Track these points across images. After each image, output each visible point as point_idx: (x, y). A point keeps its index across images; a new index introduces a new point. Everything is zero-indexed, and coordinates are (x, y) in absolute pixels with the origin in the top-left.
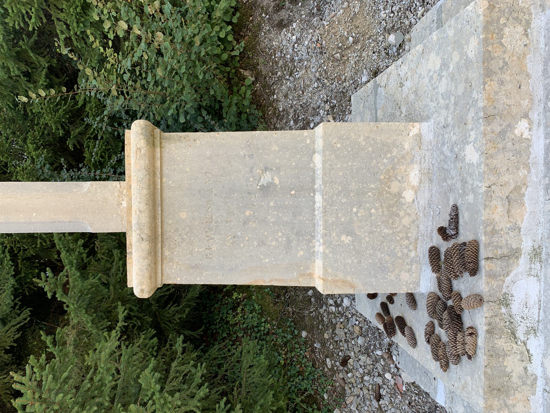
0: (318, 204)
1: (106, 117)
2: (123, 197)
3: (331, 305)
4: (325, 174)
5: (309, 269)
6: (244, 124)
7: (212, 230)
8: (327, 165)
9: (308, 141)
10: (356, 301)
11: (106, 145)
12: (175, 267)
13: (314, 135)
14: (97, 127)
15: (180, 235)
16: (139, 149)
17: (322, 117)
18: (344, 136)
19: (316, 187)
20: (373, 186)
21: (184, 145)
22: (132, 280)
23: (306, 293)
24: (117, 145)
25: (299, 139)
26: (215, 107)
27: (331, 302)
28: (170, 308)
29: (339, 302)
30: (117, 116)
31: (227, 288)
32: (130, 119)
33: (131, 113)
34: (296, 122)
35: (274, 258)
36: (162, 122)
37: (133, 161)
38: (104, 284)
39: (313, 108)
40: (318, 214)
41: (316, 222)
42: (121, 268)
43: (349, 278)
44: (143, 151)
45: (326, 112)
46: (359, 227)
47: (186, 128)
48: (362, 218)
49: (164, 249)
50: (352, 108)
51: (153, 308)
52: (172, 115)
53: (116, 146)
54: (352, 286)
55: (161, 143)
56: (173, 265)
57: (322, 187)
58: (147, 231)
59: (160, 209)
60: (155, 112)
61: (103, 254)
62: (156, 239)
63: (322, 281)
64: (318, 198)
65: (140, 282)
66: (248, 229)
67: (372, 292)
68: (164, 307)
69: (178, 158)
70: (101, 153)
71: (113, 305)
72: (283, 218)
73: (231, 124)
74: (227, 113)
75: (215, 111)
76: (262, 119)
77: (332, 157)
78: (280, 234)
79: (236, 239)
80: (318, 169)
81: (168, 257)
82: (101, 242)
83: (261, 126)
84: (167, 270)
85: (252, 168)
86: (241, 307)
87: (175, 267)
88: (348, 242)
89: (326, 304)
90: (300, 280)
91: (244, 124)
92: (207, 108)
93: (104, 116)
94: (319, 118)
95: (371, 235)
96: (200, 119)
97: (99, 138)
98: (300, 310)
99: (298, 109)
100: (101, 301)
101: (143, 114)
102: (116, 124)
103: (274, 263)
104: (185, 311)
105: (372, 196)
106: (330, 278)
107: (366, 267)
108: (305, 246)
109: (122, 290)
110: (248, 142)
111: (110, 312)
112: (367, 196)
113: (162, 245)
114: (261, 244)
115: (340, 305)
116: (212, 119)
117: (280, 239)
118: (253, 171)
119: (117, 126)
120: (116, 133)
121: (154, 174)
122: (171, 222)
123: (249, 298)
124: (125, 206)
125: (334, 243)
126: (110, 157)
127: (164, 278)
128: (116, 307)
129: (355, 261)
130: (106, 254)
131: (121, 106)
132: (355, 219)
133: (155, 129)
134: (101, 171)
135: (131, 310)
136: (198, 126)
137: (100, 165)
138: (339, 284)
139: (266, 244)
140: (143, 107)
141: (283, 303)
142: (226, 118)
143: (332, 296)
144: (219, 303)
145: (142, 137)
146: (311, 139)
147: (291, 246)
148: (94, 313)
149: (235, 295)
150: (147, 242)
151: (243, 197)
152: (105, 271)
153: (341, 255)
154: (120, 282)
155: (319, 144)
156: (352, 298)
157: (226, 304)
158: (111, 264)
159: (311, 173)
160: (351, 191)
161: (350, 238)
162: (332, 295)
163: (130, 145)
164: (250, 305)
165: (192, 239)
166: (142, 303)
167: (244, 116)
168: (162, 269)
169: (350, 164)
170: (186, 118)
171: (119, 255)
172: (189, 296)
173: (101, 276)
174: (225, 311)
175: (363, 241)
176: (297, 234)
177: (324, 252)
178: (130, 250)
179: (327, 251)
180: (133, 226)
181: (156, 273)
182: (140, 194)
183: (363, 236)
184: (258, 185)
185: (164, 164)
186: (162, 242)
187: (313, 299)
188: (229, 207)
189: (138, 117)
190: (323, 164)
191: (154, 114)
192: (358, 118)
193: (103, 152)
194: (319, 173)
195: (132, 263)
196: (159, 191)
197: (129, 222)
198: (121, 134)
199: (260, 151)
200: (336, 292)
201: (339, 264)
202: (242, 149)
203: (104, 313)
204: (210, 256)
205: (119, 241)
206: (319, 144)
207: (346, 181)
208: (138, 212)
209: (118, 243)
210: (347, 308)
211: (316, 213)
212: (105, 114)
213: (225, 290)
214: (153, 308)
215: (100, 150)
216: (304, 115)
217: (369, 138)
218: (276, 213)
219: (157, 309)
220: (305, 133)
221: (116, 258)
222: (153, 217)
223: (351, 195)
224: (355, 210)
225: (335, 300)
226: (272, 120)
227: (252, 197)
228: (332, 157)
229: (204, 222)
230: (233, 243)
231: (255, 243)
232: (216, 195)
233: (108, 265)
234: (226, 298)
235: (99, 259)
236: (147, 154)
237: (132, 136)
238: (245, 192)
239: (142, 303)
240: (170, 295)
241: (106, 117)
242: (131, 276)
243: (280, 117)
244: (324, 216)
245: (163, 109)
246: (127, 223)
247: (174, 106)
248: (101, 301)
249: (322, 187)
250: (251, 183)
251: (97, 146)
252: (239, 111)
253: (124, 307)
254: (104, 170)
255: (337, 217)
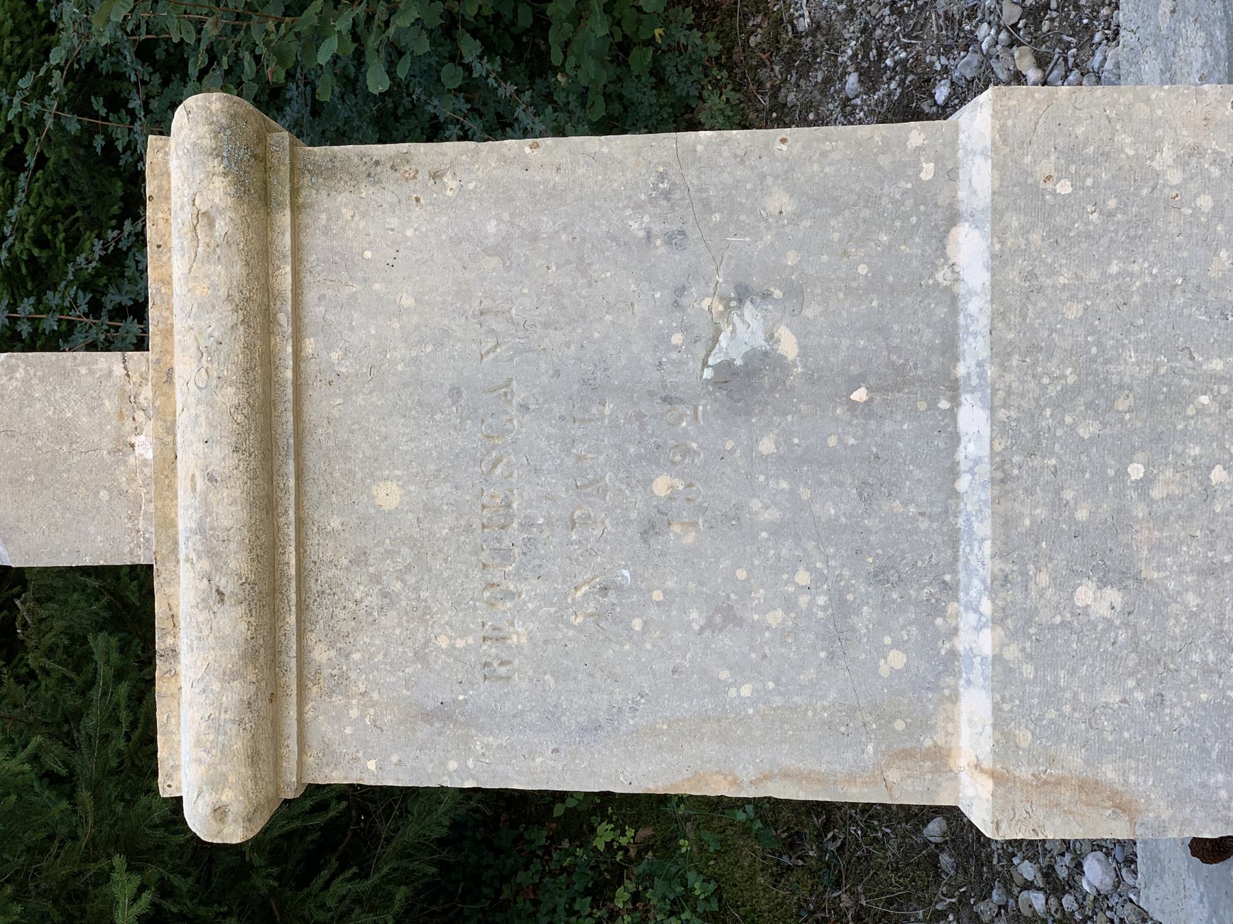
0: (971, 448)
1: (57, 74)
2: (140, 416)
3: (1028, 886)
4: (1003, 315)
5: (932, 729)
6: (642, 95)
7: (506, 556)
8: (1013, 275)
9: (928, 172)
10: (1141, 868)
11: (58, 193)
12: (354, 713)
13: (953, 144)
14: (19, 116)
15: (376, 579)
16: (205, 218)
17: (988, 56)
18: (1085, 146)
19: (961, 370)
20: (1217, 365)
21: (390, 197)
22: (176, 768)
23: (917, 830)
24: (121, 194)
25: (884, 161)
26: (514, 24)
27: (1027, 870)
28: (327, 886)
29: (1063, 873)
30: (105, 67)
31: (571, 803)
32: (156, 79)
33: (160, 54)
34: (870, 79)
35: (777, 681)
36: (293, 91)
37: (178, 265)
38: (51, 778)
39: (948, 18)
40: (972, 488)
41: (961, 522)
42: (124, 715)
43: (1109, 773)
44: (222, 226)
45: (1003, 36)
46: (1157, 547)
47: (399, 120)
48: (1168, 506)
49: (312, 638)
50: (1121, 17)
51: (257, 881)
52: (336, 58)
53: (100, 195)
54: (1123, 806)
55: (295, 192)
56: (347, 706)
57: (990, 371)
58: (238, 561)
59: (291, 467)
60: (261, 50)
61: (50, 652)
62: (277, 593)
63: (989, 784)
64: (973, 419)
65: (206, 775)
66: (662, 554)
67: (1210, 832)
68: (303, 881)
69: (368, 254)
70: (38, 227)
71: (93, 868)
72: (817, 508)
73: (583, 95)
74: (567, 44)
75: (516, 38)
76: (721, 67)
77: (1035, 237)
78: (803, 577)
79: (612, 597)
80: (972, 293)
81: (327, 672)
82: (38, 601)
83: (715, 101)
84: (322, 726)
85: (681, 290)
86: (631, 887)
87: (354, 713)
88: (1107, 613)
89: (1008, 882)
90: (893, 775)
91: (642, 95)
92: (482, 24)
93: (49, 71)
94: (972, 58)
95: (1211, 582)
96: (451, 76)
97: (31, 161)
98: (889, 903)
99: (880, 21)
100: (40, 849)
101: (213, 58)
102: (98, 104)
103: (778, 701)
104: (390, 897)
105: (1215, 408)
106: (1024, 772)
107: (1185, 721)
108: (914, 630)
109: (129, 804)
110: (662, 177)
111: (79, 896)
112: (1190, 411)
113: (299, 621)
114: (718, 619)
115: (1071, 885)
116: (504, 77)
117: (804, 600)
118: (684, 301)
119: (103, 112)
120: (99, 142)
121: (266, 318)
122: (335, 523)
123: (666, 846)
124: (149, 455)
125: (1044, 616)
126: (73, 245)
127: (310, 760)
128: (104, 877)
129: (1139, 696)
130: (59, 653)
131: (122, 26)
132: (1140, 511)
133: (270, 130)
134: (39, 301)
135: (165, 890)
136: (444, 107)
137: (32, 277)
138: (1065, 796)
139: (739, 622)
140: (211, 30)
141: (812, 873)
142: (562, 69)
143: (1032, 849)
144: (537, 865)
145: (216, 165)
146: (938, 160)
147: (853, 629)
148: (14, 899)
149: (604, 834)
150: (241, 610)
151: (640, 416)
152: (59, 725)
153: (1073, 672)
154: (116, 772)
155: (978, 180)
156: (1122, 855)
157: (563, 870)
158: (83, 693)
159: (941, 312)
160: (1121, 387)
161: (1113, 595)
162: (1031, 842)
163: (167, 199)
164: (669, 879)
165: (424, 595)
166: (211, 860)
167: (641, 59)
168: (301, 721)
169: (1114, 269)
170: (391, 73)
171: (115, 656)
172: (410, 833)
173: (40, 745)
174: (562, 902)
175: (1174, 608)
176: (878, 576)
177: (997, 659)
178: (170, 641)
179: (1012, 653)
180: (181, 540)
181: (276, 739)
182: (211, 405)
183: (1171, 585)
184: (705, 364)
185: (308, 278)
186: (302, 607)
187: (945, 860)
188: (580, 458)
189: (193, 71)
190: (993, 272)
191: (257, 59)
192: (1150, 65)
193: (44, 221)
194: (976, 309)
195: (176, 696)
196: (290, 391)
197: (167, 524)
198: (120, 146)
199: (717, 217)
200: (1055, 829)
201: (1067, 709)
202: (639, 207)
203: (55, 902)
204: (503, 670)
205: (121, 602)
206: (978, 180)
207: (1099, 344)
208: (200, 484)
209: (109, 607)
210: (1100, 897)
211: (963, 484)
212: (53, 63)
213: (559, 810)
214: (257, 881)
215: (33, 211)
216: (905, 47)
217: (1202, 155)
218: (784, 485)
219: (271, 889)
220: (915, 133)
221: (104, 672)
222: (265, 504)
223: (1122, 405)
224: (1136, 471)
225: (1044, 862)
226: (763, 73)
227: (681, 418)
228: (1035, 237)
229: (477, 524)
230: (598, 616)
231: (694, 615)
232: (524, 408)
233: (71, 701)
234: (566, 844)
235: (32, 675)
236: (239, 237)
237: (173, 164)
238: (651, 394)
239: (211, 860)
240: (332, 827)
241: (57, 74)
242: (175, 751)
243: (797, 59)
244: (996, 500)
245: (298, 35)
246: (158, 526)
247: (343, 24)
248: (40, 849)
249: (990, 371)
250: (674, 355)
251: (21, 196)
252: (618, 39)
253: (136, 880)
254: (52, 299)
255: (1057, 504)
